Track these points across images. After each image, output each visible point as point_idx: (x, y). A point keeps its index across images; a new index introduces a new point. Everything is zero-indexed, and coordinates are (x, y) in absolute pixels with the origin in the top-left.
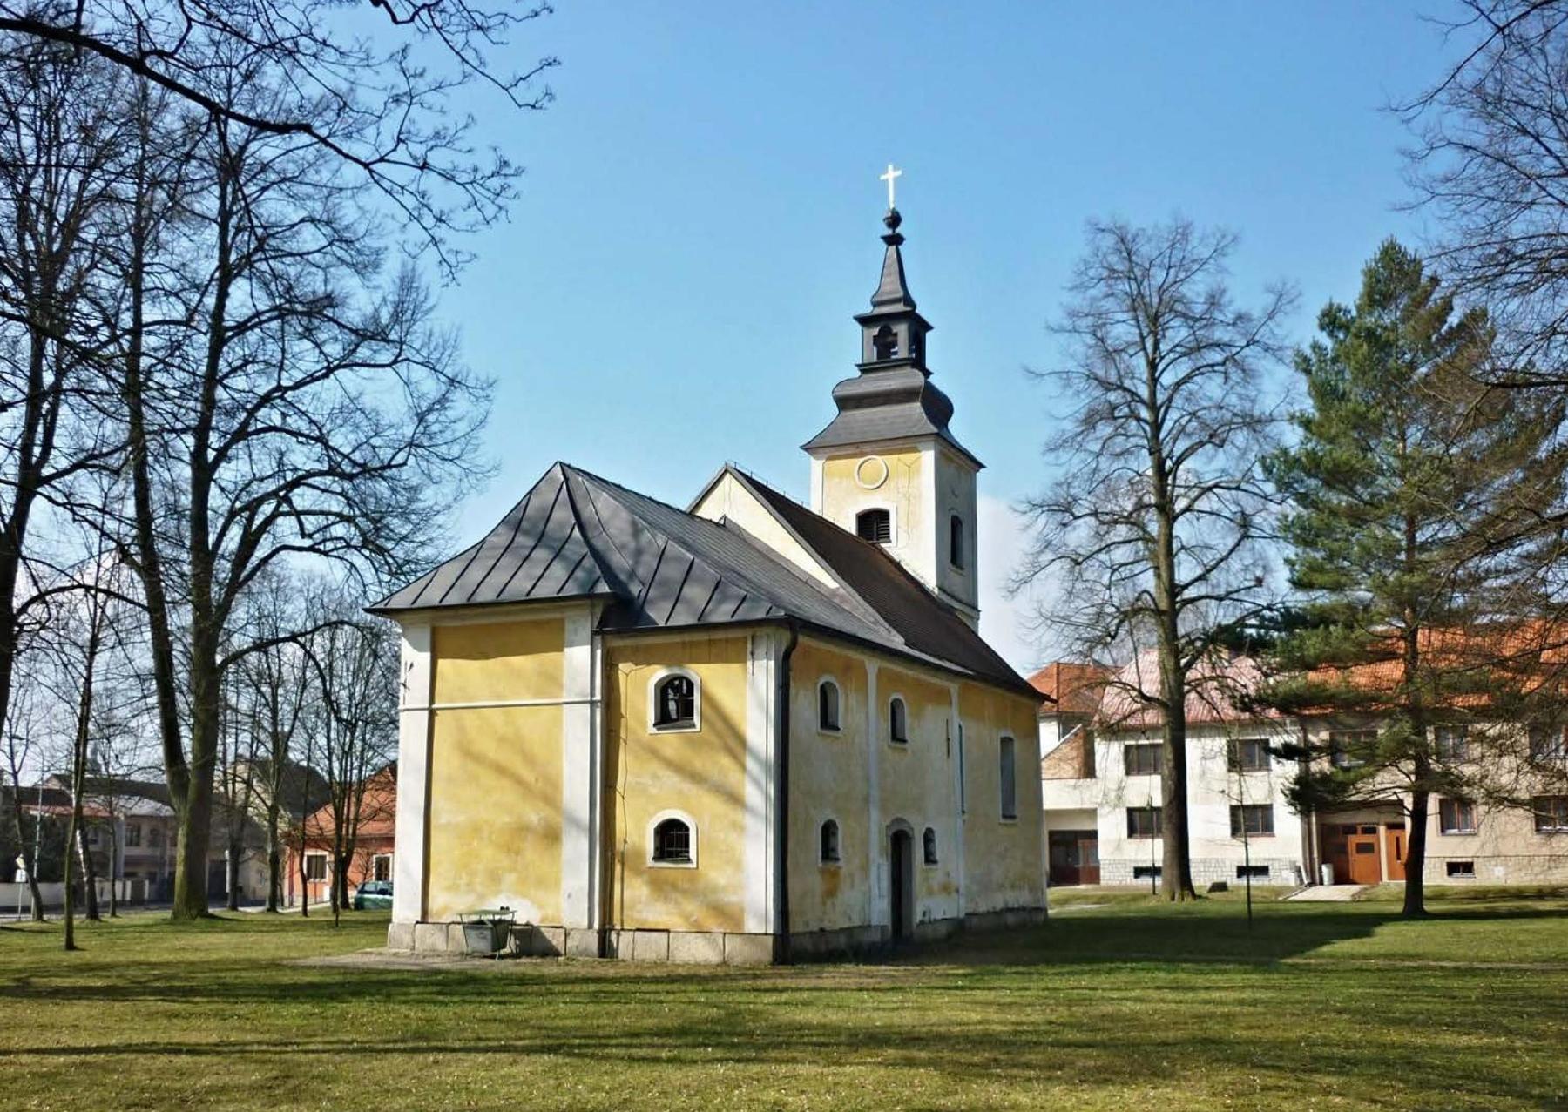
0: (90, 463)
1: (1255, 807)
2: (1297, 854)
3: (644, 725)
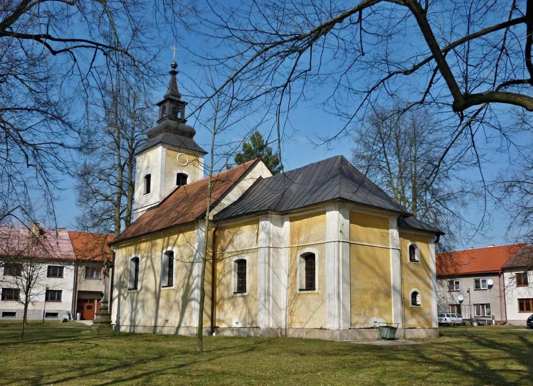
0: (44, 40)
1: (55, 291)
2: (70, 309)
3: (406, 259)
